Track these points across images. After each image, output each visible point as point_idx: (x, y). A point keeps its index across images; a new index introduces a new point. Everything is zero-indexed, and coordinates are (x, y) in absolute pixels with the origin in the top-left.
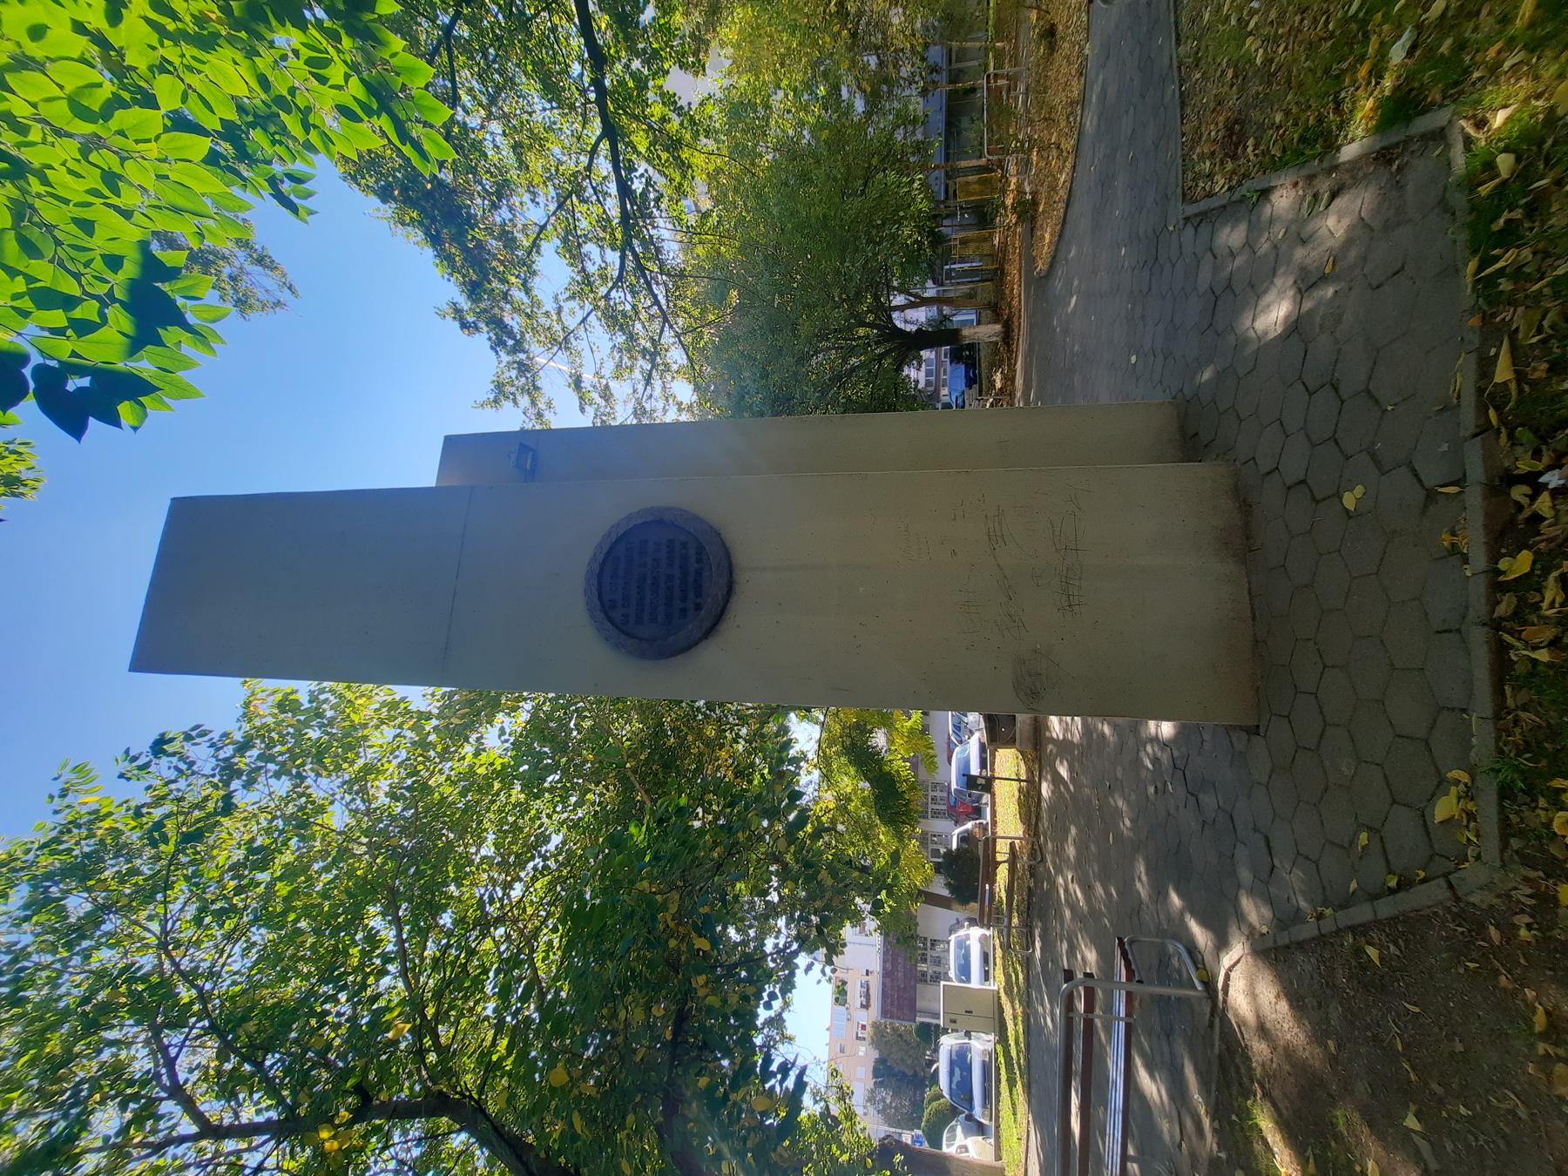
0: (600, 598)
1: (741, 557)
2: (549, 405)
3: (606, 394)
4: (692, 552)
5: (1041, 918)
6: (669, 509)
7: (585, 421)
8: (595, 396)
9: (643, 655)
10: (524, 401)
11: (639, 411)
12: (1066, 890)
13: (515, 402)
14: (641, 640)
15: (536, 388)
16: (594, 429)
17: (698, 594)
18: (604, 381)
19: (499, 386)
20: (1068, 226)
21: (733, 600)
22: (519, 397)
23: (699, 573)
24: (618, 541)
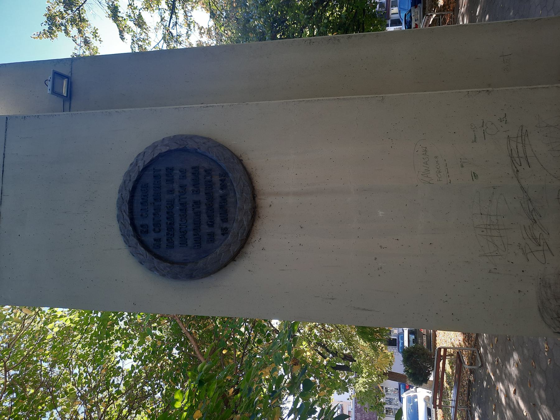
0: (133, 224)
1: (262, 182)
2: (95, 34)
3: (140, 23)
4: (216, 179)
5: (479, 404)
6: (192, 137)
7: (124, 47)
8: (131, 24)
9: (175, 277)
10: (74, 31)
11: (168, 37)
12: (507, 396)
13: (67, 32)
14: (172, 263)
15: (83, 20)
16: (133, 54)
17: (225, 220)
18: (137, 12)
19: (51, 19)
20: (6, 149)
21: (245, 161)
22: (69, 28)
23: (224, 198)
24: (145, 168)
